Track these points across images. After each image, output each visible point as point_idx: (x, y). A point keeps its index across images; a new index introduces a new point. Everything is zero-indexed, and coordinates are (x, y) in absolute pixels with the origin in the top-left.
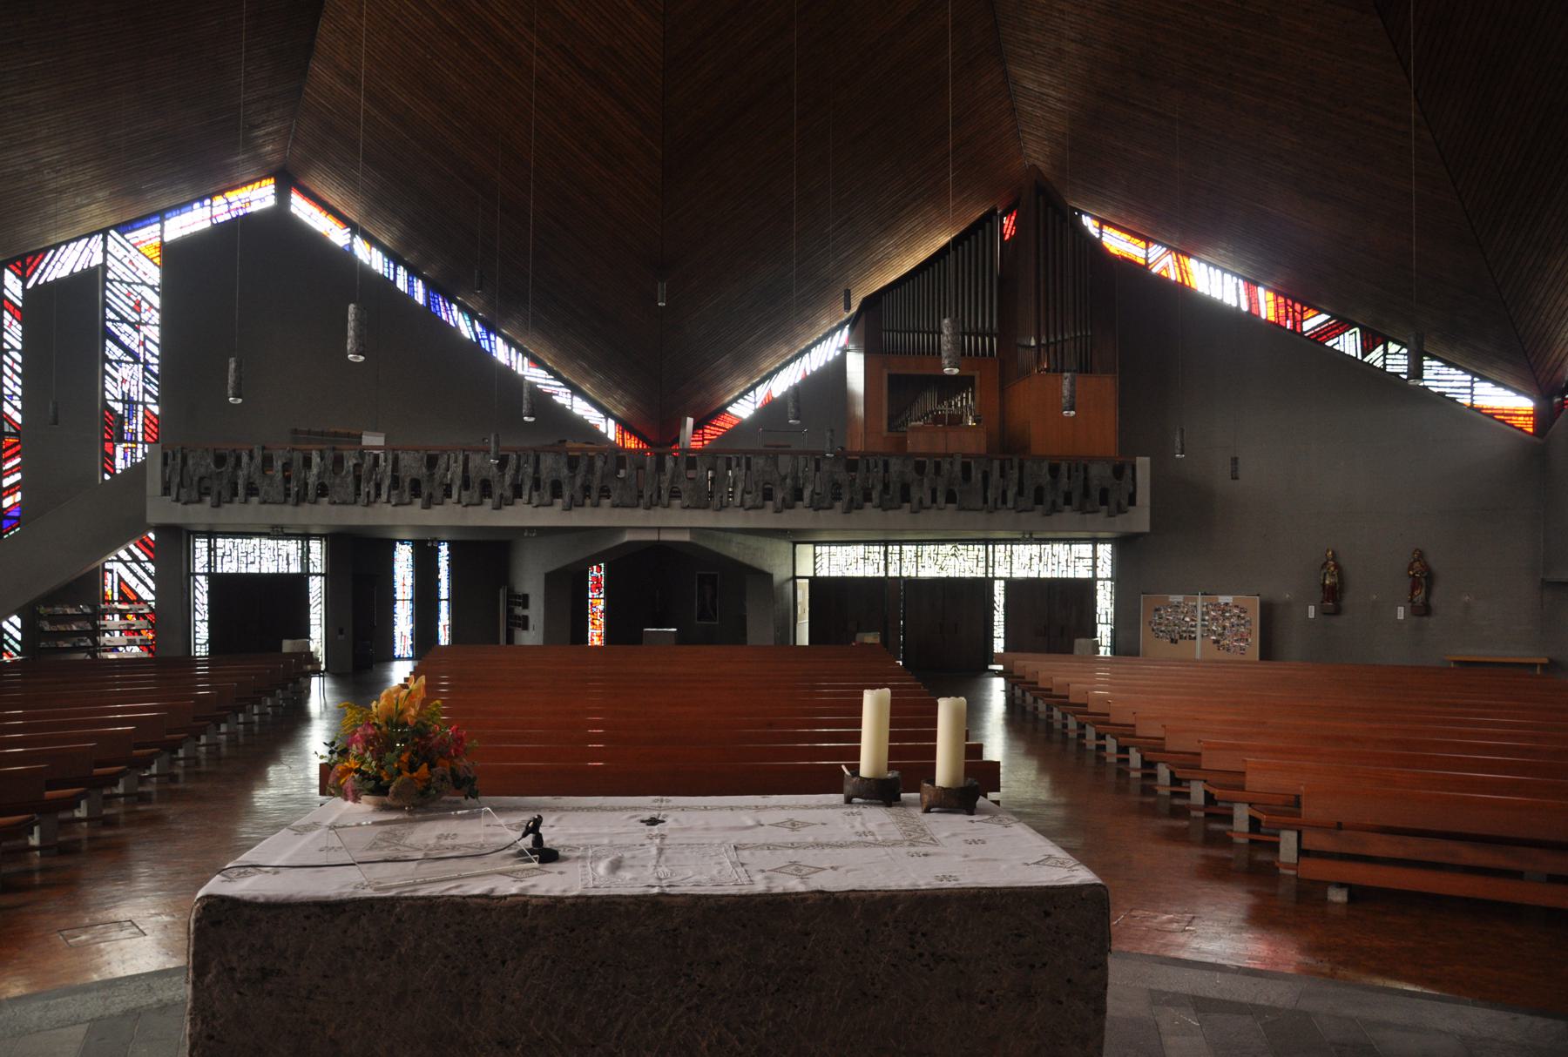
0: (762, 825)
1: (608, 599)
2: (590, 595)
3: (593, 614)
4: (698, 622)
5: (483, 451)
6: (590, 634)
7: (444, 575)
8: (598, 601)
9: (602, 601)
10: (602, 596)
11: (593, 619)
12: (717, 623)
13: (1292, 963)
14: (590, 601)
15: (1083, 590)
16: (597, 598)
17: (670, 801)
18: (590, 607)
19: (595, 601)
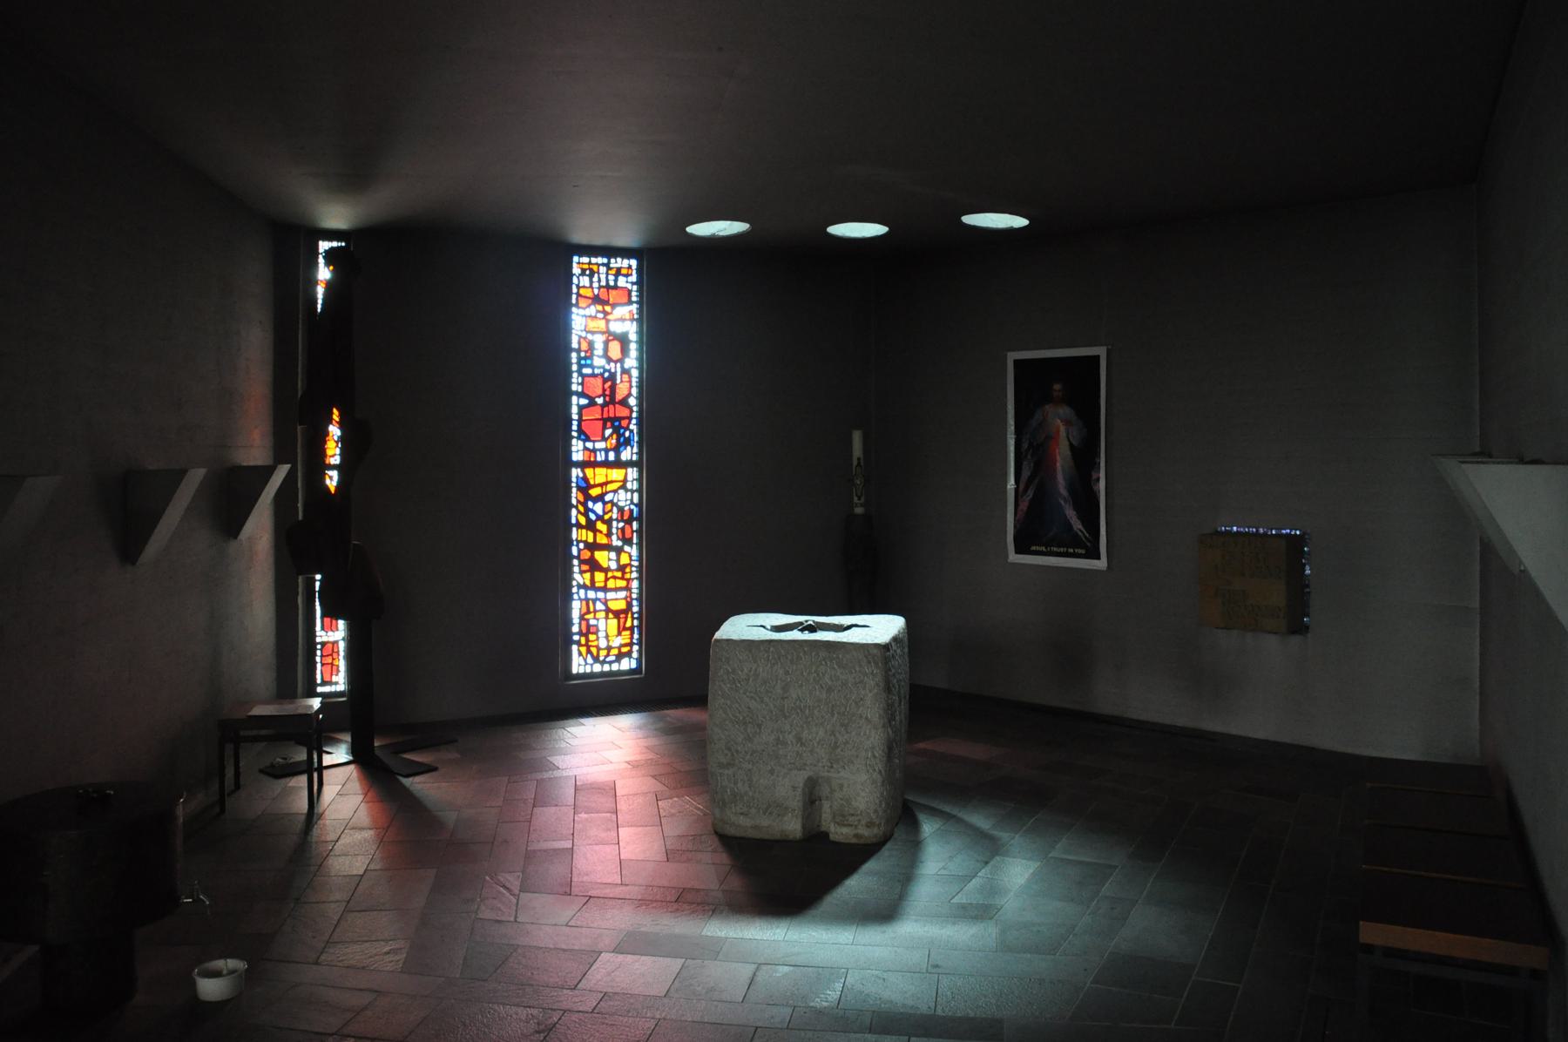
0: (611, 762)
1: (656, 469)
2: (578, 451)
3: (590, 526)
4: (1014, 557)
5: (353, 1037)
6: (576, 608)
7: (1012, 448)
8: (617, 474)
9: (632, 473)
10: (626, 455)
11: (593, 547)
12: (1101, 564)
13: (583, 596)
14: (576, 473)
15: (1097, 358)
16: (606, 464)
17: (714, 950)
18: (575, 496)
19: (599, 475)
